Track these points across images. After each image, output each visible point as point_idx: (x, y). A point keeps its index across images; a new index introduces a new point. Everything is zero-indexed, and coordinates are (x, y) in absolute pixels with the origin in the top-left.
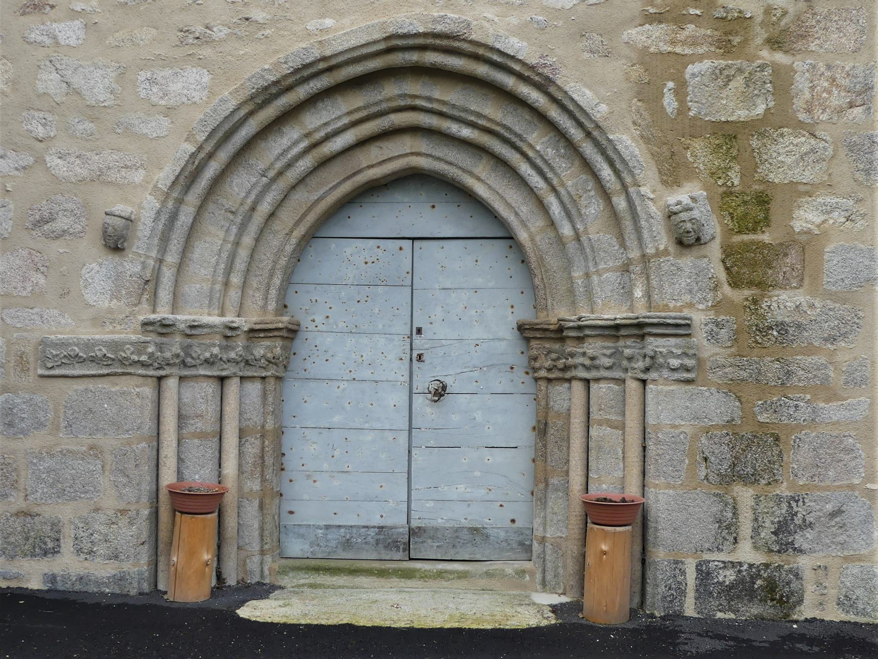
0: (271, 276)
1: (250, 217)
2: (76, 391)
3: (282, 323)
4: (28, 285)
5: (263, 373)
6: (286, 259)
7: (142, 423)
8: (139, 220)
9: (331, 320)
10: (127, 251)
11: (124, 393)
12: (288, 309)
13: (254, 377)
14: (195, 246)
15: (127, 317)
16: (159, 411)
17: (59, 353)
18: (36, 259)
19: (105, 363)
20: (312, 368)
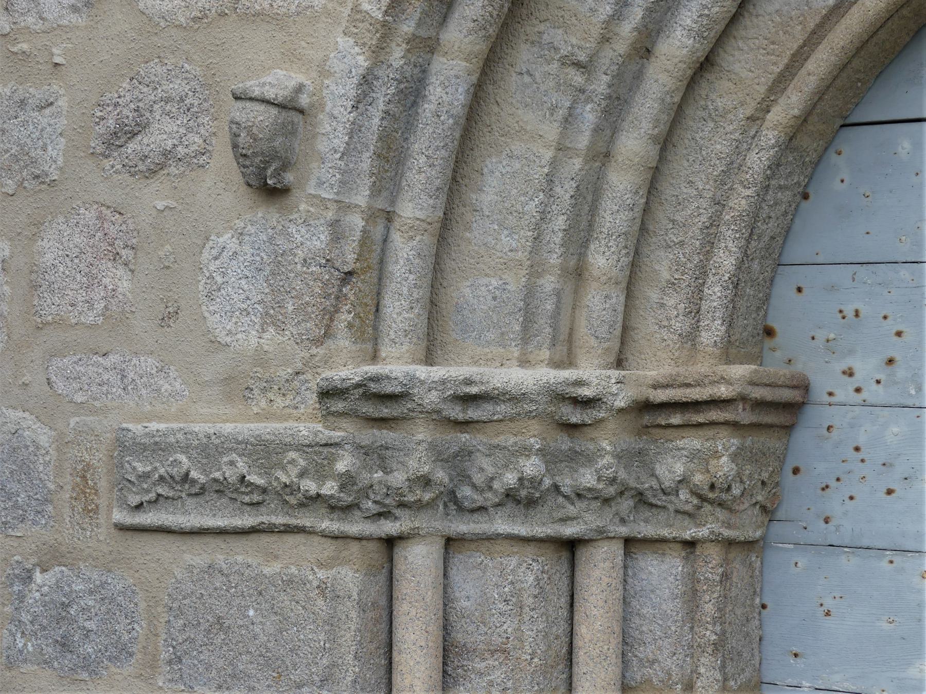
0: (709, 244)
1: (639, 76)
2: (190, 568)
3: (728, 382)
4: (98, 294)
5: (686, 528)
6: (748, 192)
7: (334, 665)
8: (322, 106)
9: (900, 372)
10: (296, 193)
11: (291, 581)
12: (778, 340)
13: (663, 541)
14: (485, 170)
15: (297, 373)
16: (390, 632)
17: (149, 468)
18: (112, 230)
19: (247, 499)
20: (845, 513)
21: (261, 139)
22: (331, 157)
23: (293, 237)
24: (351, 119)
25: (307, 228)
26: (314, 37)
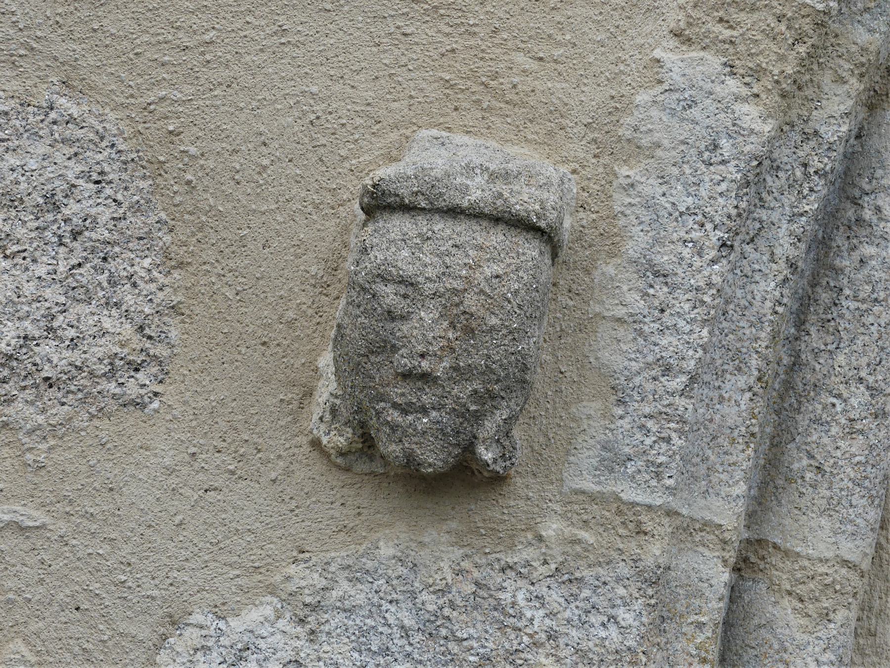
21: (492, 329)
22: (649, 386)
23: (520, 616)
24: (716, 279)
25: (564, 590)
26: (559, 44)
